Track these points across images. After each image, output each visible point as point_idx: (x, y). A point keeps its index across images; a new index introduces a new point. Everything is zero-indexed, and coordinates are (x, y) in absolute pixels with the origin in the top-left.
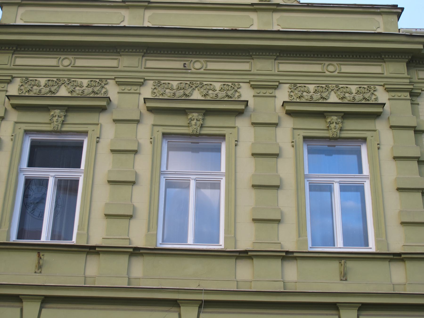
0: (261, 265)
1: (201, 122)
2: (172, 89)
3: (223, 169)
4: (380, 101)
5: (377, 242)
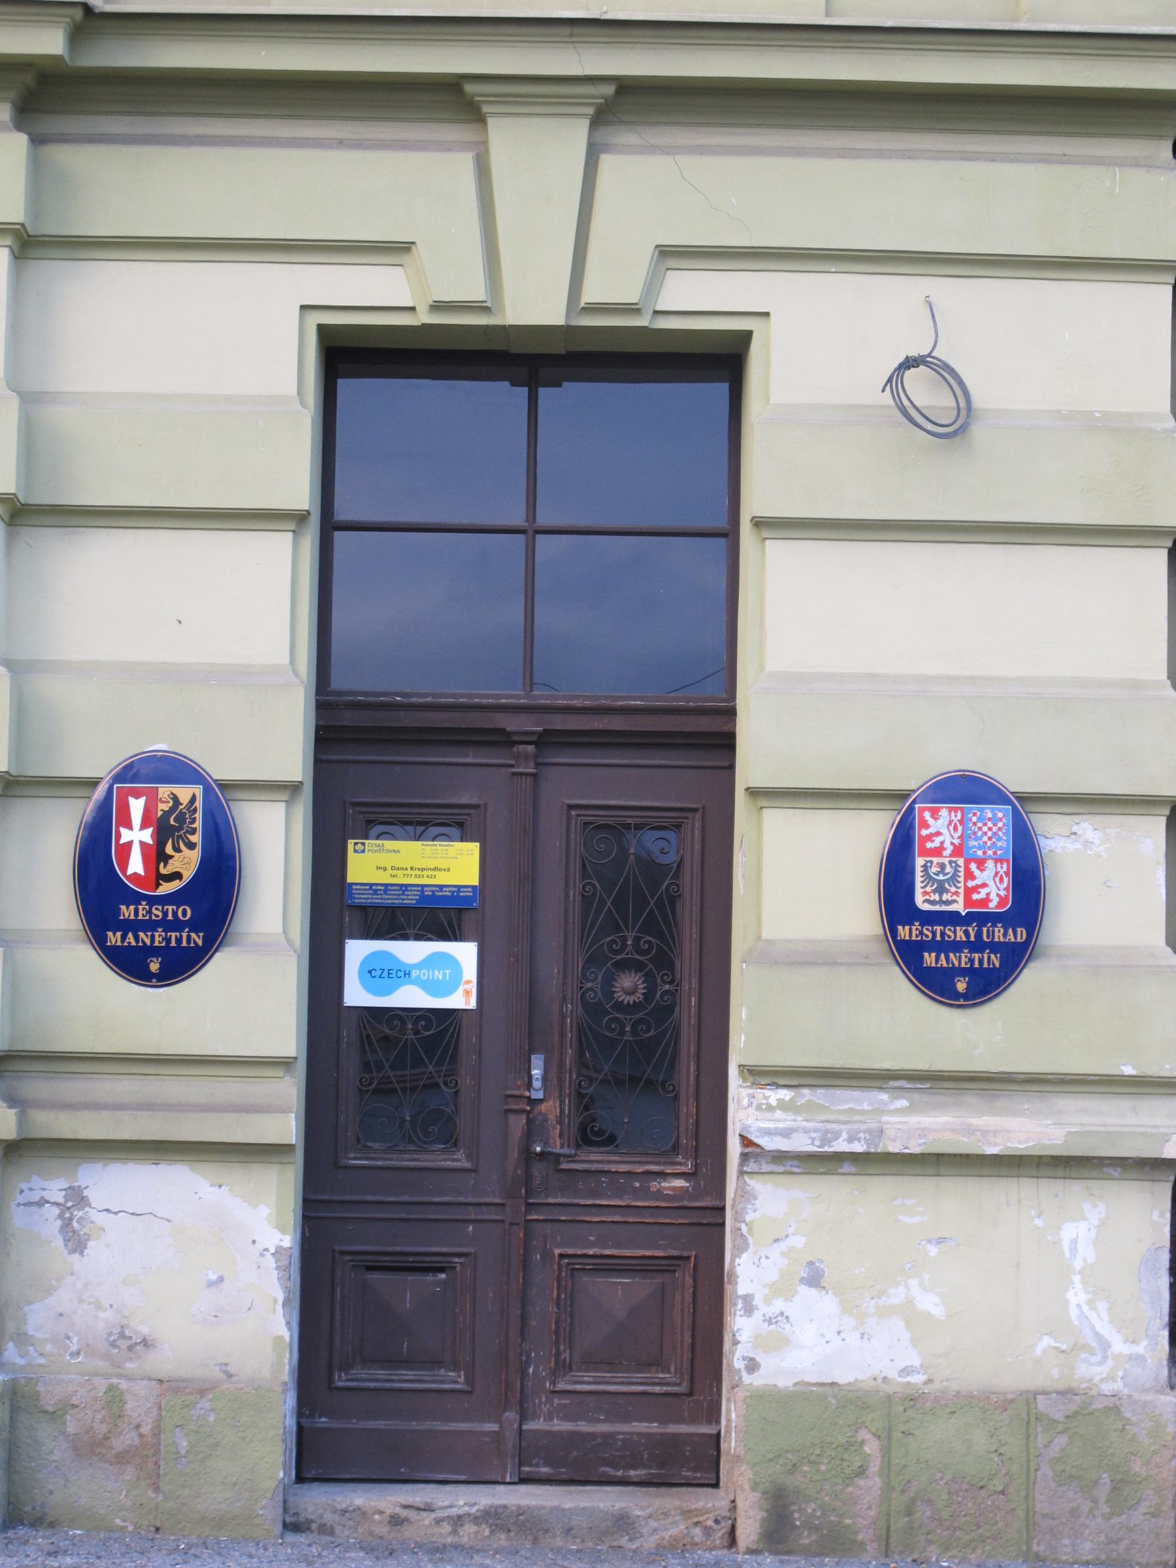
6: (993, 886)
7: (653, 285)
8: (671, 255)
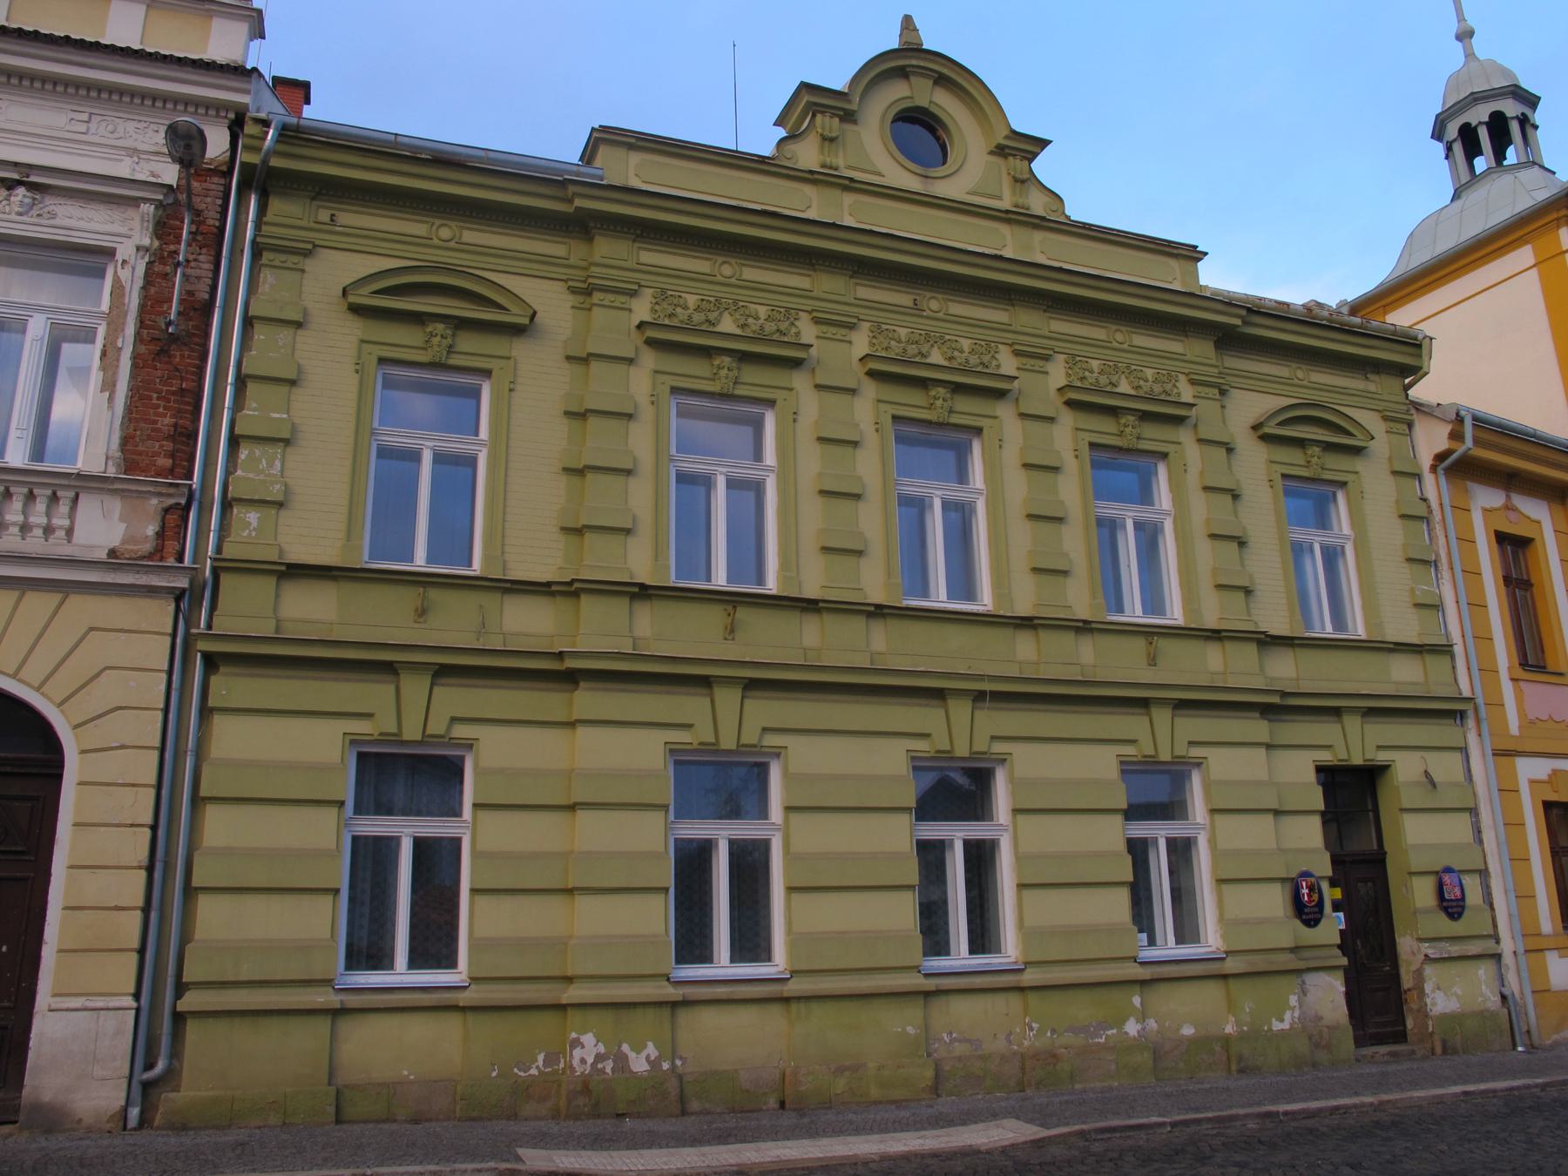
0: (832, 622)
1: (449, 340)
2: (899, 342)
3: (484, 433)
4: (804, 341)
5: (487, 558)
6: (1458, 893)
7: (760, 739)
8: (1379, 747)
